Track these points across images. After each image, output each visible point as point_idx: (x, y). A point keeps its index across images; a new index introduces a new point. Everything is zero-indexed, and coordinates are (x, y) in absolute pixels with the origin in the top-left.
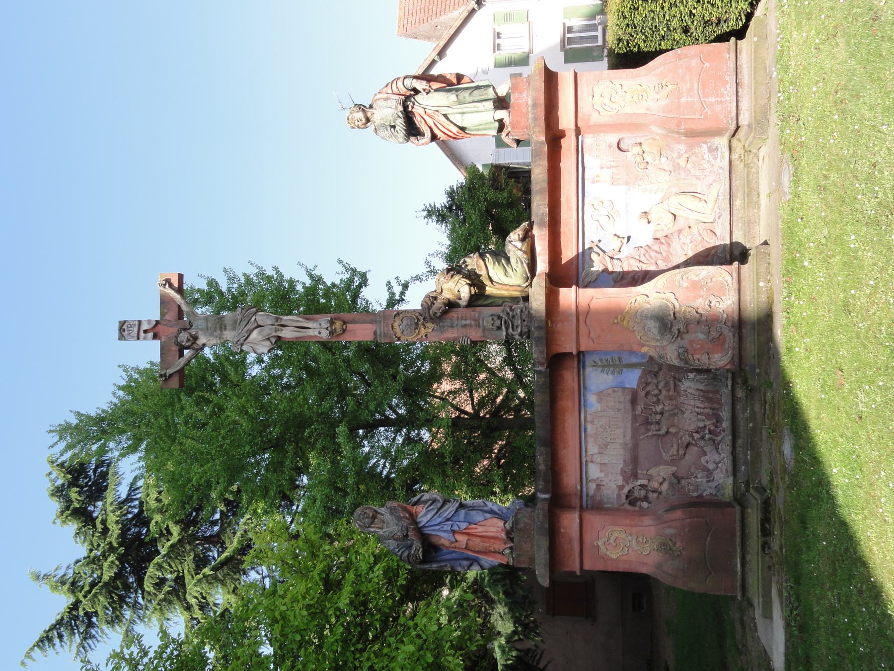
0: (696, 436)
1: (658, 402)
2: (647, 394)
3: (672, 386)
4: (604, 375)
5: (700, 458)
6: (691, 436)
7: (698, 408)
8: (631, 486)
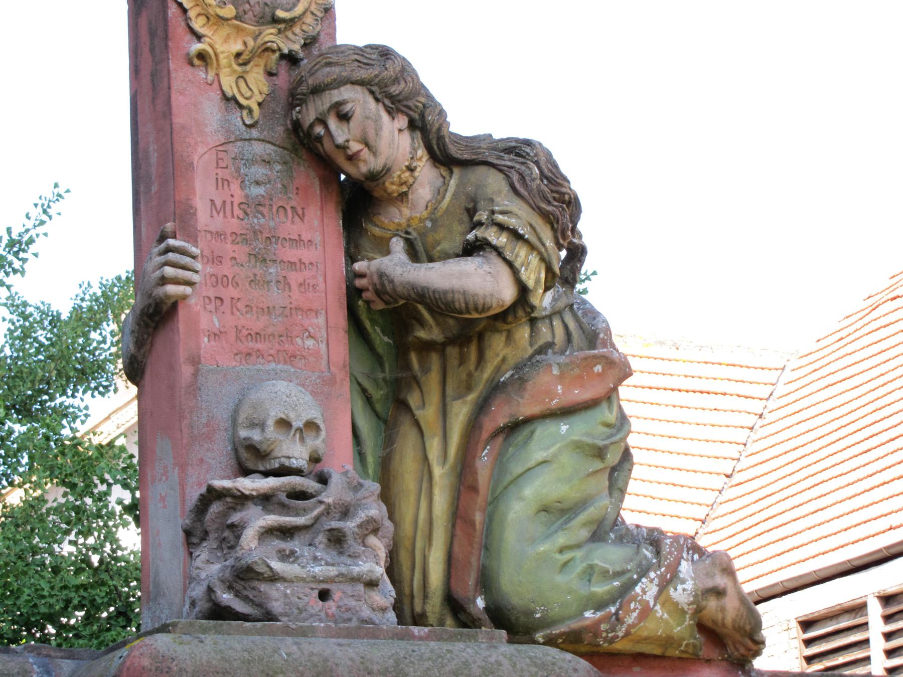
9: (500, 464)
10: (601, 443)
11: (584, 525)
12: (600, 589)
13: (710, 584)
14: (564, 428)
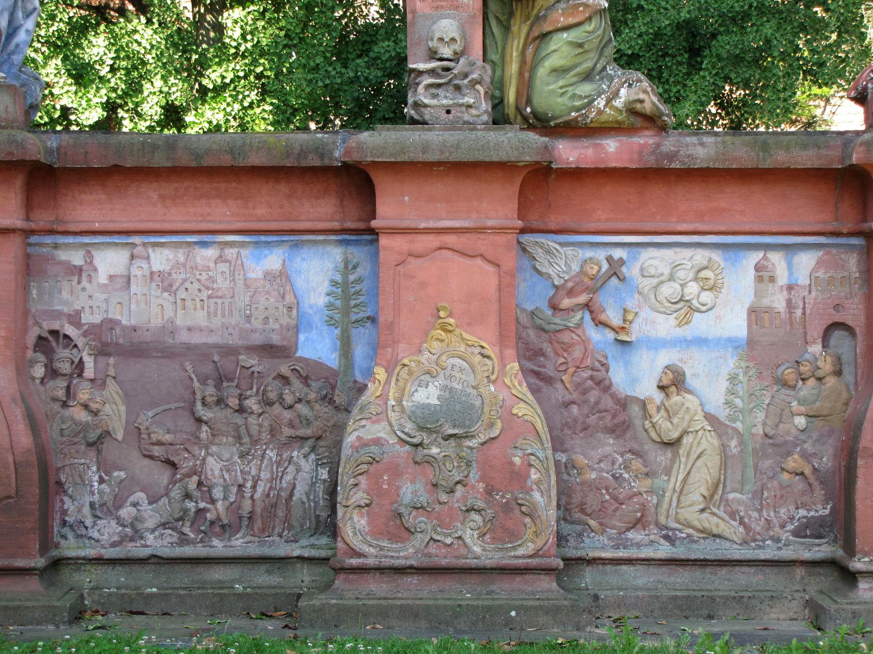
2: (285, 380)
3: (302, 432)
4: (325, 287)
6: (194, 472)
7: (254, 487)
8: (80, 342)
9: (537, 50)
10: (580, 41)
11: (575, 76)
12: (577, 103)
13: (636, 97)
14: (565, 35)
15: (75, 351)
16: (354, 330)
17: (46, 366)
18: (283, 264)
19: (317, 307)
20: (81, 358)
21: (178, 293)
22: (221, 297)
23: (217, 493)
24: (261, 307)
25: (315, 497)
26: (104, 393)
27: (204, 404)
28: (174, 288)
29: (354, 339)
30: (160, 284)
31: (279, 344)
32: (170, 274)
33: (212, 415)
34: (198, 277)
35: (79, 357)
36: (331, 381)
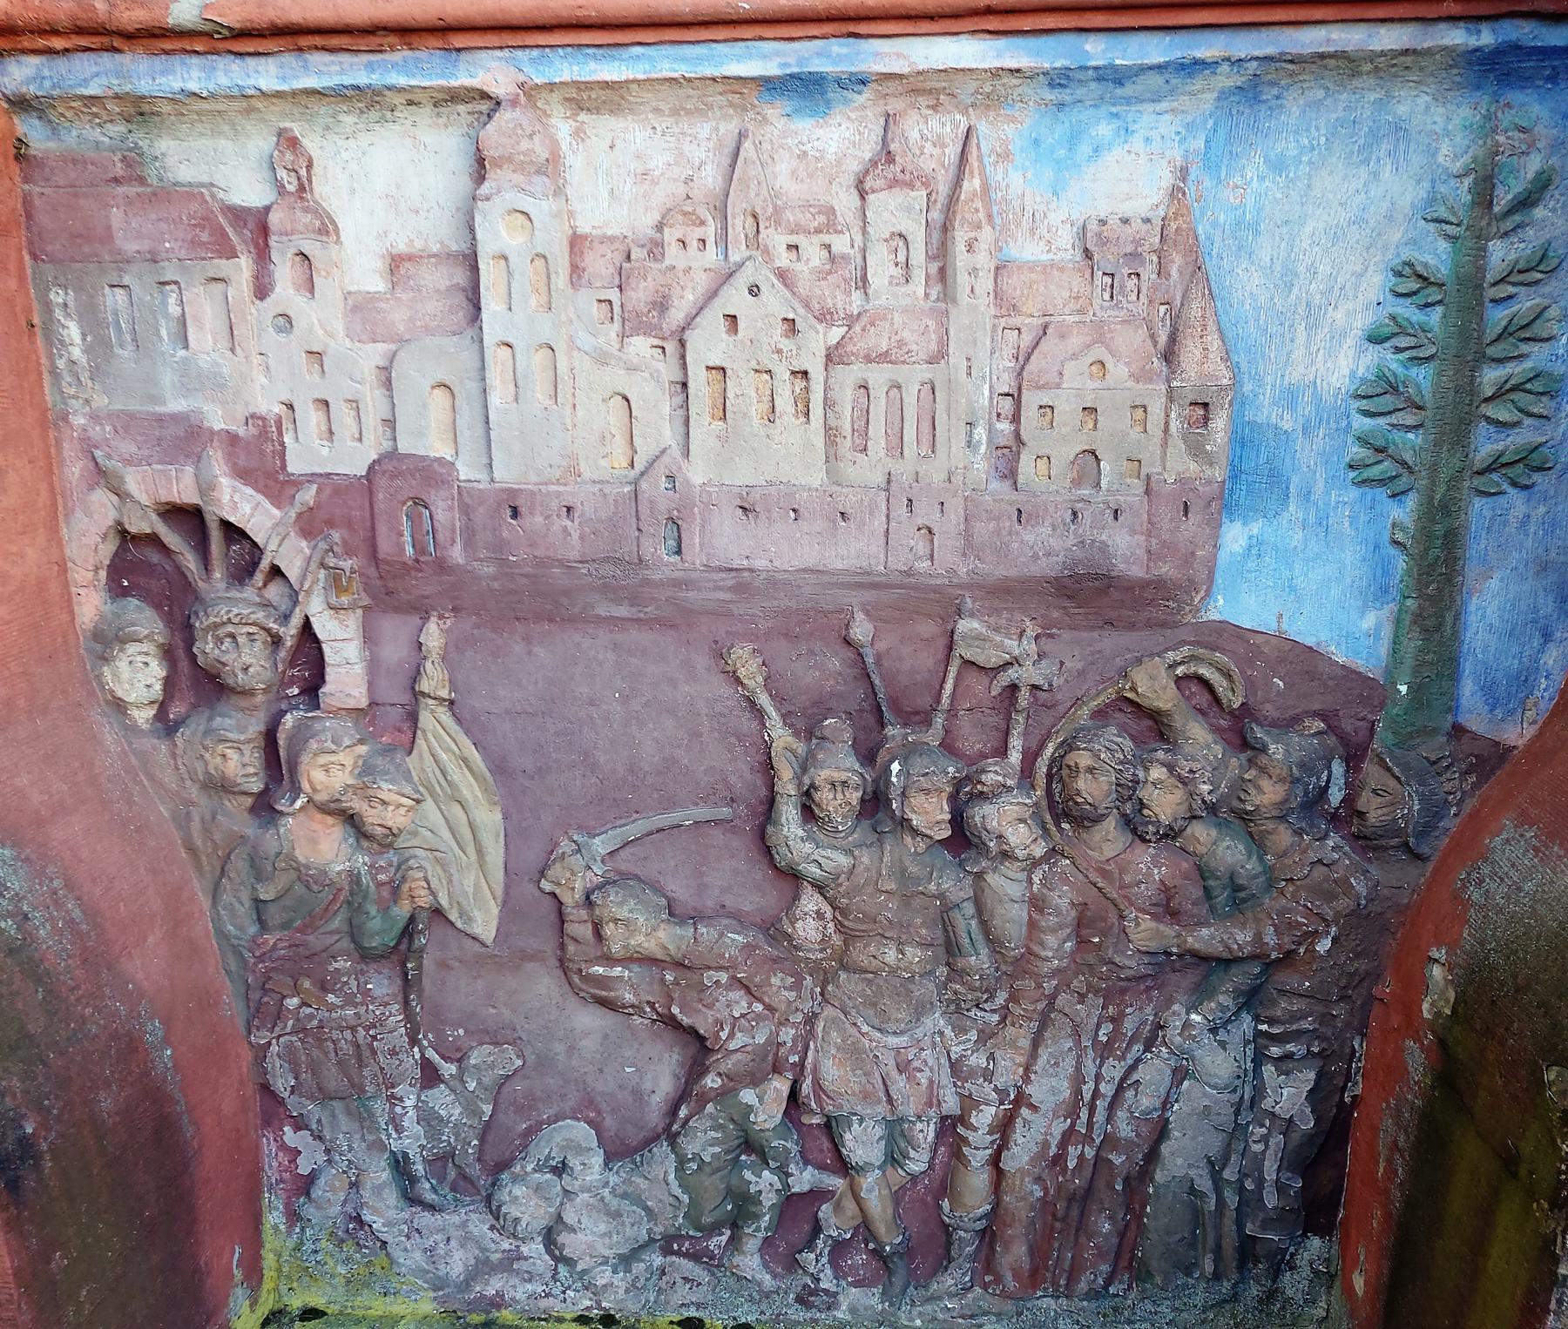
0: (765, 1105)
1: (1063, 811)
2: (1155, 728)
3: (1205, 938)
4: (1365, 297)
5: (588, 1109)
6: (769, 1063)
7: (1004, 1126)
8: (291, 554)
15: (274, 592)
16: (1478, 502)
17: (168, 654)
18: (1176, 193)
19: (1317, 399)
20: (307, 625)
21: (694, 339)
22: (884, 357)
23: (863, 1144)
24: (1067, 407)
25: (1243, 1175)
26: (411, 762)
27: (809, 812)
28: (677, 315)
29: (1477, 546)
30: (614, 295)
31: (1137, 572)
32: (655, 249)
33: (844, 861)
34: (784, 259)
35: (296, 621)
36: (1348, 725)
